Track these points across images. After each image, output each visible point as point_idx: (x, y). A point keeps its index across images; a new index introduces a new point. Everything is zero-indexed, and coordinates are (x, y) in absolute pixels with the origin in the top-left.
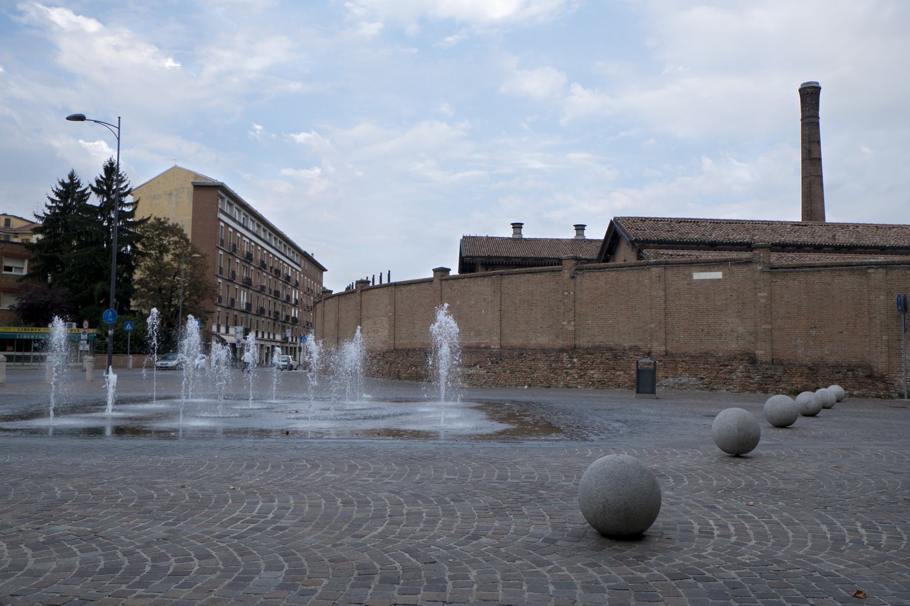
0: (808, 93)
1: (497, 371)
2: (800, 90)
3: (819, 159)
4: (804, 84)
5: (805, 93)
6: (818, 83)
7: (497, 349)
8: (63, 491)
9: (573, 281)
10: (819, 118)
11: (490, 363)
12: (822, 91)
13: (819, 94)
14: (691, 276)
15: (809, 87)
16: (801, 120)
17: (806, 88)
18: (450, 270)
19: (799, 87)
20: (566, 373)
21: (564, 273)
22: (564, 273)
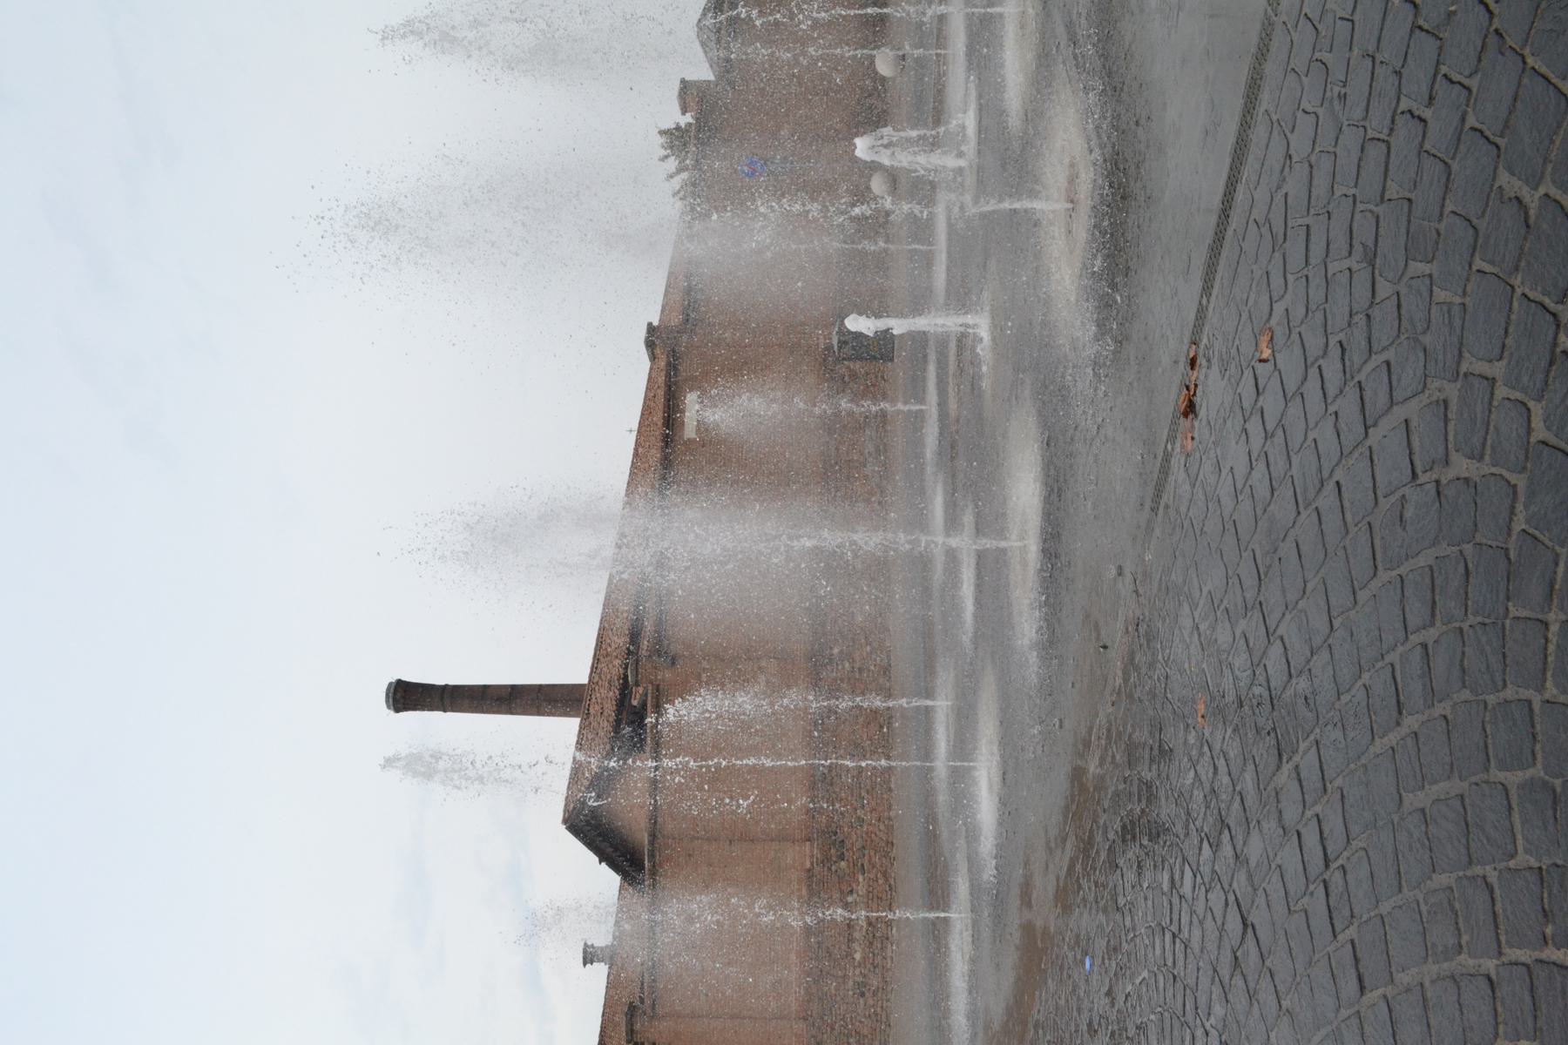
0: (404, 698)
1: (858, 845)
2: (397, 710)
3: (513, 687)
4: (387, 701)
5: (402, 701)
6: (390, 684)
7: (812, 846)
8: (1548, 921)
9: (680, 663)
10: (446, 685)
11: (843, 864)
12: (403, 679)
13: (409, 683)
14: (691, 441)
15: (395, 693)
16: (445, 711)
17: (394, 699)
18: (650, 324)
19: (392, 713)
20: (860, 670)
21: (663, 680)
22: (663, 680)
